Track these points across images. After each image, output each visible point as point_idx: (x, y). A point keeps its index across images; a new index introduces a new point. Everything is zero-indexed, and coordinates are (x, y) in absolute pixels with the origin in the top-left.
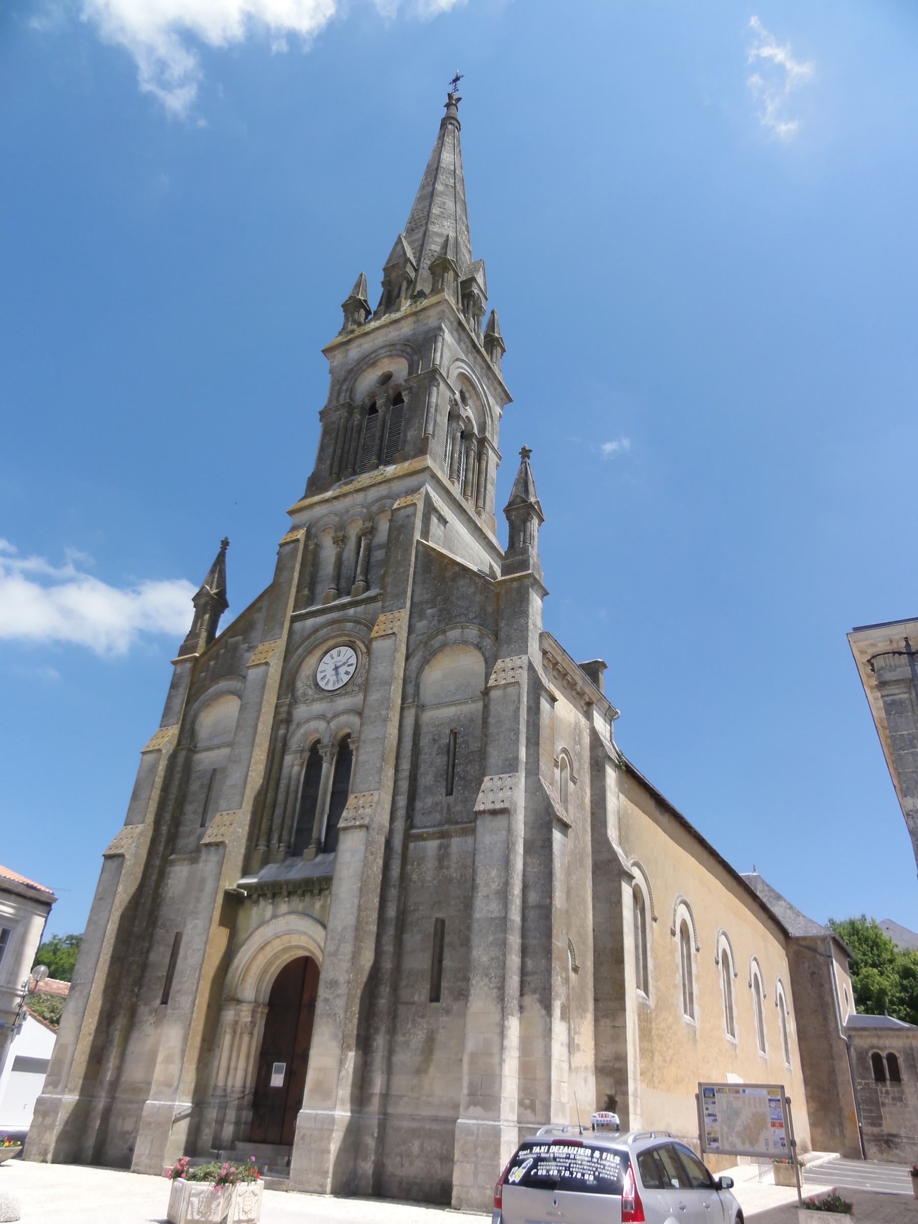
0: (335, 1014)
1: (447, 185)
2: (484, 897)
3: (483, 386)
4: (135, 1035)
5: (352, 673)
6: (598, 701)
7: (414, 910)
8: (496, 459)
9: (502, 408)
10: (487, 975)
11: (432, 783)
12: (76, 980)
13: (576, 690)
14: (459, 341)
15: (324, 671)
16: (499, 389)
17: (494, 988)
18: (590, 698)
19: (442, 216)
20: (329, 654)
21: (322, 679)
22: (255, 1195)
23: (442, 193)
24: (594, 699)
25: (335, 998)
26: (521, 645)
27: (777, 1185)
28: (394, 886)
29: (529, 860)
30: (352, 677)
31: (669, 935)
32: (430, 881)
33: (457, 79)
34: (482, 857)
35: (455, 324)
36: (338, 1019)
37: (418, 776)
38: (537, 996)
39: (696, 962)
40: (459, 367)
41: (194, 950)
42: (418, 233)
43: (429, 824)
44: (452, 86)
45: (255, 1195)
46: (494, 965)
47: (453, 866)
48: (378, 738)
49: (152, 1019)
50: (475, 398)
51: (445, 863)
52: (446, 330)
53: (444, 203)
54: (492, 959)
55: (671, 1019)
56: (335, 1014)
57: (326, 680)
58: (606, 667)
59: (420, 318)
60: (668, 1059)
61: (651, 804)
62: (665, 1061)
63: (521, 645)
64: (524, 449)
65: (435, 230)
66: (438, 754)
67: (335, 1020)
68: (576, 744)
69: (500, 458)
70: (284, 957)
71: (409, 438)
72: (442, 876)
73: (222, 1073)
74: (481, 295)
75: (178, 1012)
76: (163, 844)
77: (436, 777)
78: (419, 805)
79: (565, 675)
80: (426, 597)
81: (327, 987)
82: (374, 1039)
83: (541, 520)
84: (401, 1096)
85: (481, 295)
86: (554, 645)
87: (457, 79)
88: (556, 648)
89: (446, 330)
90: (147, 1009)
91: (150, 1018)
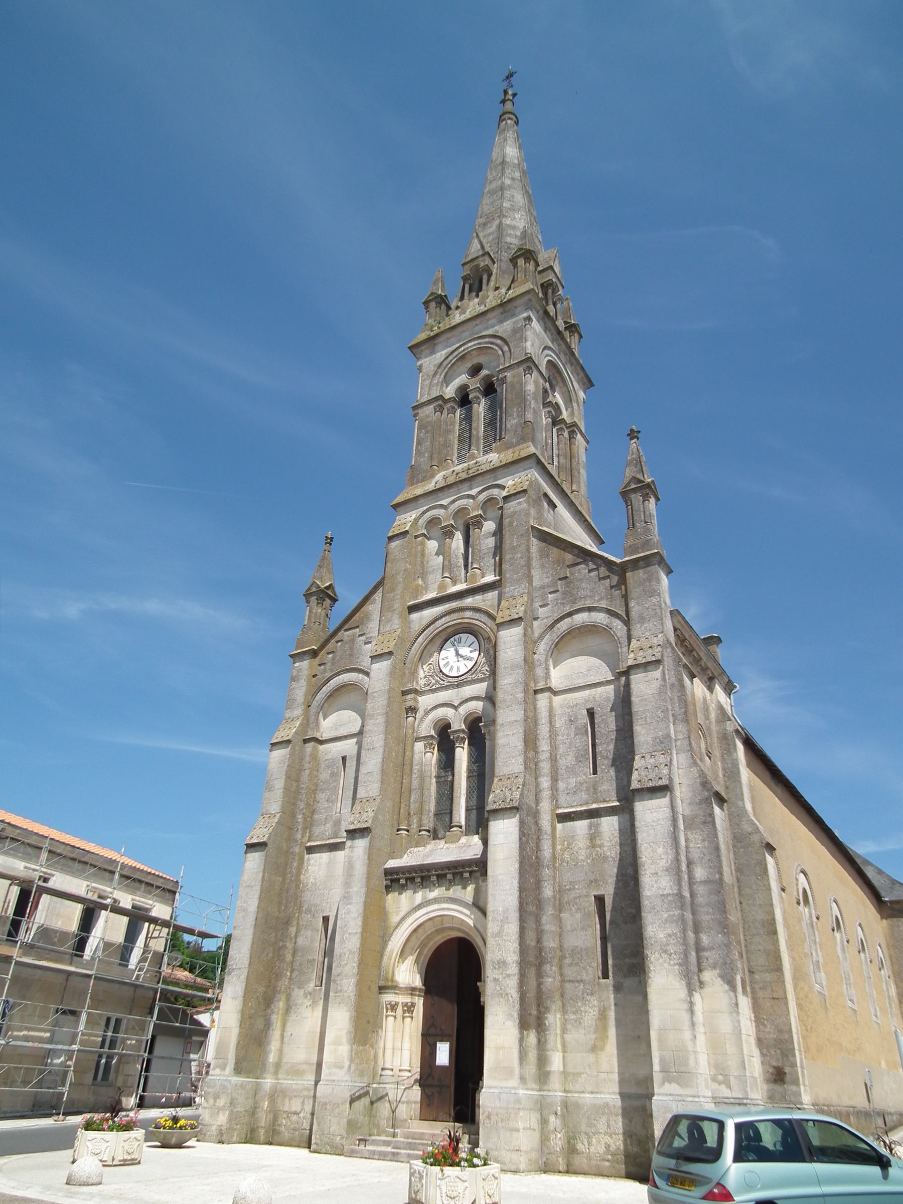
0: (507, 994)
1: (513, 179)
2: (653, 874)
3: (568, 372)
4: (293, 1017)
5: (476, 659)
6: (720, 675)
7: (570, 890)
8: (585, 443)
9: (585, 393)
10: (665, 952)
11: (573, 763)
12: (232, 965)
13: (701, 665)
14: (546, 329)
15: (446, 658)
16: (582, 375)
17: (675, 965)
18: (712, 673)
19: (512, 209)
20: (449, 641)
21: (444, 665)
22: (496, 1178)
23: (510, 187)
24: (716, 675)
25: (504, 978)
26: (655, 623)
27: (421, 1119)
28: (548, 866)
29: (690, 836)
30: (476, 663)
31: (796, 905)
32: (583, 861)
33: (511, 75)
34: (644, 835)
35: (541, 312)
36: (510, 998)
37: (558, 757)
38: (718, 971)
39: (818, 931)
40: (547, 356)
41: (350, 934)
42: (491, 227)
43: (575, 804)
44: (506, 83)
45: (496, 1178)
46: (672, 941)
47: (607, 844)
48: (516, 721)
49: (308, 1002)
50: (561, 384)
51: (598, 842)
52: (534, 319)
53: (513, 196)
54: (670, 936)
55: (806, 988)
56: (507, 994)
57: (450, 667)
58: (721, 641)
59: (506, 309)
60: (809, 1028)
61: (767, 775)
62: (807, 1030)
63: (655, 623)
64: (632, 430)
65: (508, 223)
66: (576, 735)
67: (508, 1000)
68: (706, 720)
69: (588, 442)
70: (436, 939)
71: (508, 426)
72: (596, 855)
73: (389, 1053)
74: (558, 283)
75: (341, 994)
76: (300, 831)
77: (577, 758)
78: (561, 785)
79: (692, 651)
80: (546, 580)
81: (495, 968)
82: (546, 1018)
83: (657, 499)
84: (579, 1074)
85: (558, 283)
86: (682, 622)
87: (511, 75)
88: (684, 624)
89: (534, 319)
90: (302, 992)
91: (305, 1001)
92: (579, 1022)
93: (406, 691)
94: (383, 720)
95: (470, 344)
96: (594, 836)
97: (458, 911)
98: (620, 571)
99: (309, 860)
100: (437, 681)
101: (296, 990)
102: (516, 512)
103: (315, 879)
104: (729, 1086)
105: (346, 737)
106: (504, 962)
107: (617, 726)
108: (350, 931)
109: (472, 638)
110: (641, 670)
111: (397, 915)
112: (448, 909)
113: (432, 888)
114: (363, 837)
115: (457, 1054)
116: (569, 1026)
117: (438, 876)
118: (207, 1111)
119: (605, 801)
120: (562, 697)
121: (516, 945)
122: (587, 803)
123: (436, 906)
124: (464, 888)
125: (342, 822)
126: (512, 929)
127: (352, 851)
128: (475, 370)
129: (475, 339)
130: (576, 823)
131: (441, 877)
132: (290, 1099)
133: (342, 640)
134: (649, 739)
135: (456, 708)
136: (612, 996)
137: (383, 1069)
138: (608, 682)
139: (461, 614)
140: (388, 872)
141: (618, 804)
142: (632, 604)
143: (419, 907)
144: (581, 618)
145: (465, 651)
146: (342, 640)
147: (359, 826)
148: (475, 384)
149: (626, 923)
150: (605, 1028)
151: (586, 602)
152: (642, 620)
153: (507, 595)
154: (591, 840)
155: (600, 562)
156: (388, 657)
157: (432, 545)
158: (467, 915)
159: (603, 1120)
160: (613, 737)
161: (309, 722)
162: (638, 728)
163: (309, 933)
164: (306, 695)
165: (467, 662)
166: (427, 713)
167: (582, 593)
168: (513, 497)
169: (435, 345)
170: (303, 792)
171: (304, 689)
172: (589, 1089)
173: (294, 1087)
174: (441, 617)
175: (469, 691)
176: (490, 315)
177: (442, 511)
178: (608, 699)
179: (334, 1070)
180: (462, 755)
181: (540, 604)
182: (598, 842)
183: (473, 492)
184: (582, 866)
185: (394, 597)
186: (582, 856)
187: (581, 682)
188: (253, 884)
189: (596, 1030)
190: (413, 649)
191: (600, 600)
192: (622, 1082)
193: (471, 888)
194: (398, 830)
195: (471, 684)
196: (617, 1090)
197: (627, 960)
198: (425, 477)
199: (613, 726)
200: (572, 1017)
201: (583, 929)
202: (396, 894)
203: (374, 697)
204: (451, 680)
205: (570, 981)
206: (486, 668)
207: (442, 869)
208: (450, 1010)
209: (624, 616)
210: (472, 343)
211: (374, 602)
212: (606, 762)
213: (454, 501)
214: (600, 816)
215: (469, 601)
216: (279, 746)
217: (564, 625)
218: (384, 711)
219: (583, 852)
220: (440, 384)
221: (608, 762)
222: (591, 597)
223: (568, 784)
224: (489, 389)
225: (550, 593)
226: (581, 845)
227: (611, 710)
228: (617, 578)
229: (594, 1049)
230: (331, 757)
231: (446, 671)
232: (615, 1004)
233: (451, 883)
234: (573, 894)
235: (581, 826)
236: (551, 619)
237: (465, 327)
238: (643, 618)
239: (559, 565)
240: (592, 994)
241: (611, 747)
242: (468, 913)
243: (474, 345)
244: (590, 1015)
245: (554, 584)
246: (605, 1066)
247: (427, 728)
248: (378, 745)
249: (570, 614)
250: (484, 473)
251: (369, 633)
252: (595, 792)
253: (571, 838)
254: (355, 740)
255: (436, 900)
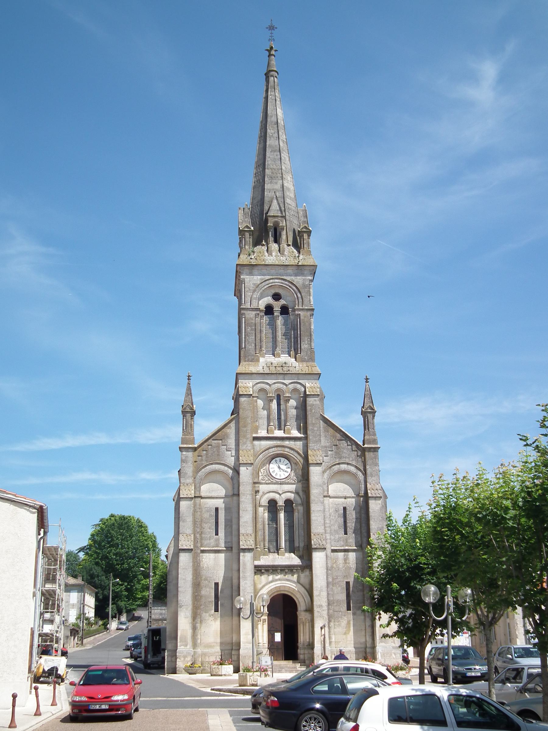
49: (212, 618)
77: (339, 527)
84: (340, 642)
92: (340, 625)
93: (255, 482)
94: (251, 497)
95: (276, 281)
96: (346, 559)
97: (290, 584)
99: (202, 556)
100: (269, 479)
101: (204, 614)
105: (217, 498)
106: (321, 605)
107: (356, 516)
108: (248, 591)
109: (286, 461)
112: (285, 583)
113: (277, 575)
114: (249, 552)
115: (285, 637)
117: (281, 570)
119: (350, 546)
120: (332, 499)
123: (279, 582)
125: (220, 540)
127: (244, 558)
128: (277, 297)
129: (279, 279)
132: (209, 657)
133: (211, 445)
134: (376, 527)
135: (280, 495)
137: (258, 643)
138: (353, 497)
139: (283, 449)
141: (356, 548)
142: (368, 467)
143: (272, 582)
144: (344, 467)
145: (283, 467)
146: (211, 445)
148: (277, 306)
149: (358, 592)
150: (350, 627)
151: (346, 460)
152: (372, 476)
153: (311, 448)
155: (353, 442)
157: (260, 403)
160: (354, 521)
162: (372, 522)
163: (208, 589)
164: (193, 472)
165: (285, 473)
166: (264, 494)
167: (344, 455)
174: (272, 448)
176: (289, 268)
177: (268, 387)
178: (352, 504)
180: (282, 516)
184: (341, 570)
185: (246, 430)
186: (341, 566)
188: (187, 567)
191: (352, 460)
192: (354, 644)
195: (287, 484)
196: (353, 646)
197: (358, 605)
198: (253, 359)
199: (354, 516)
200: (337, 623)
201: (341, 593)
202: (259, 576)
203: (244, 485)
204: (277, 480)
205: (336, 611)
207: (282, 567)
209: (362, 470)
210: (278, 281)
211: (230, 428)
213: (275, 383)
215: (287, 443)
217: (336, 468)
219: (341, 565)
220: (257, 299)
221: (352, 531)
222: (348, 458)
223: (335, 537)
225: (329, 451)
226: (341, 562)
227: (354, 510)
228: (360, 452)
229: (345, 634)
231: (274, 475)
232: (353, 619)
234: (337, 580)
235: (341, 555)
237: (270, 266)
238: (372, 475)
239: (333, 438)
240: (345, 616)
241: (354, 525)
242: (295, 585)
243: (279, 282)
244: (344, 622)
245: (331, 447)
246: (349, 639)
247: (264, 501)
249: (339, 464)
253: (337, 559)
255: (279, 580)
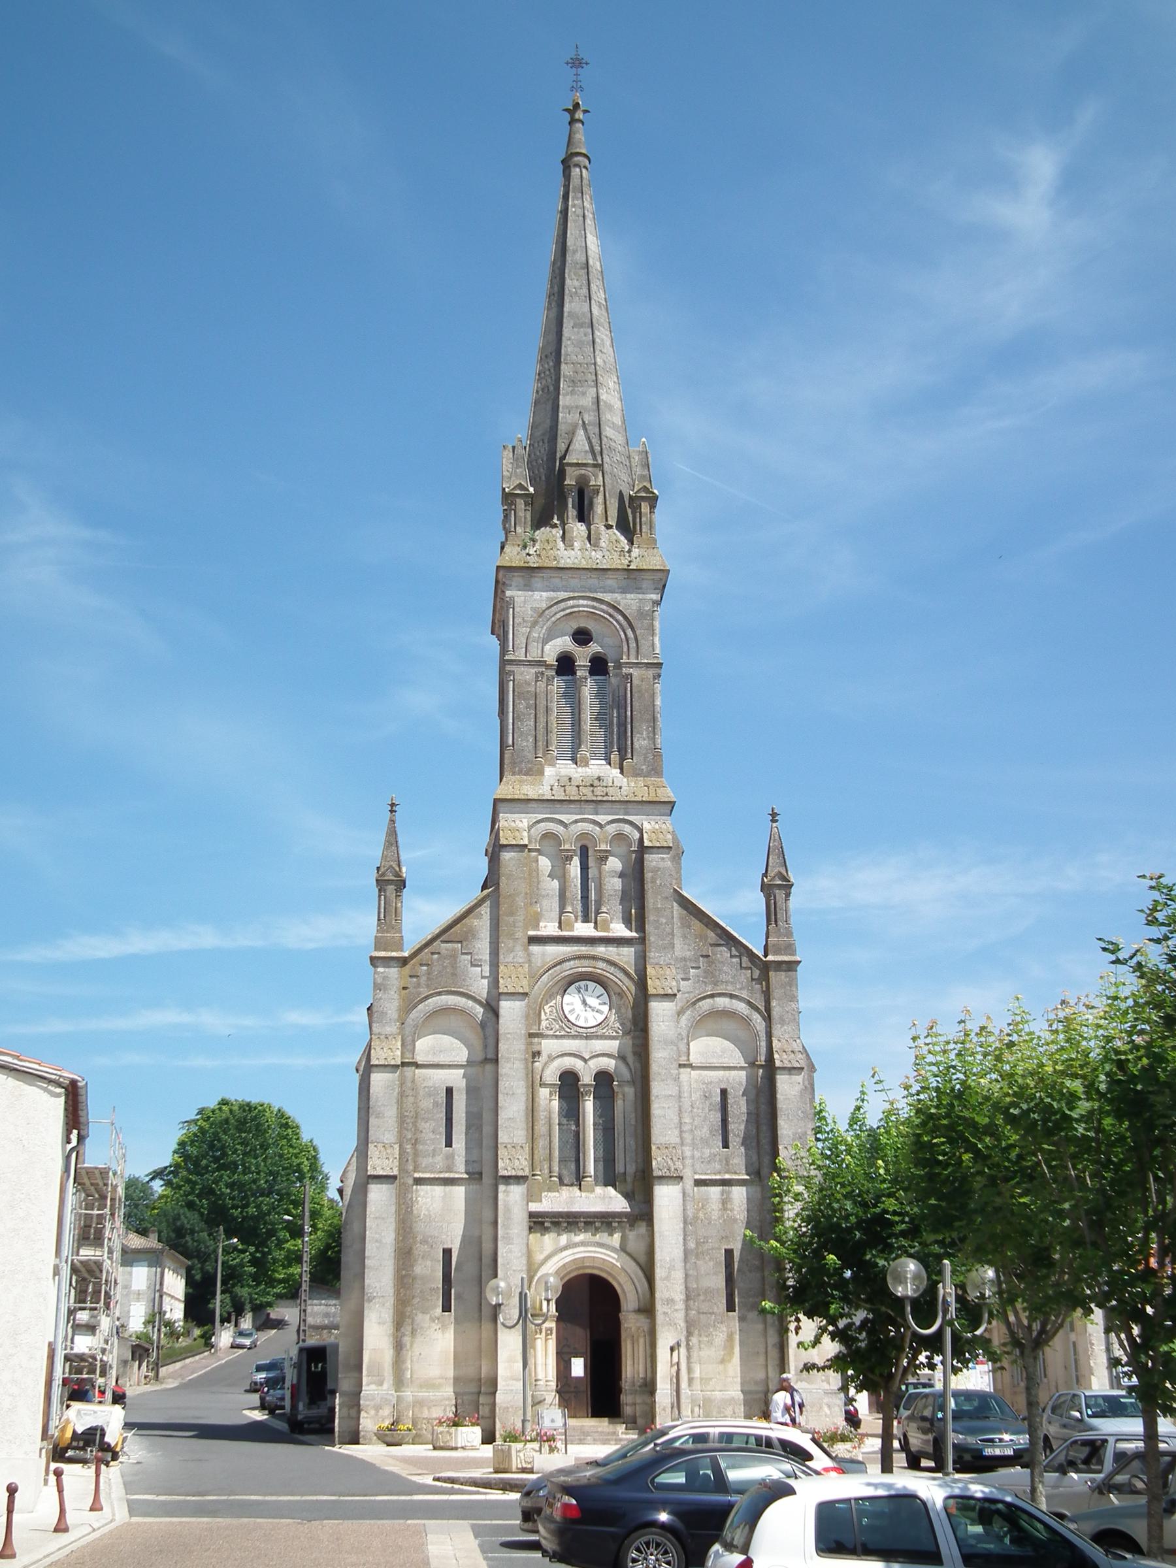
48: (671, 1096)
51: (729, 1206)
77: (711, 1131)
84: (711, 1379)
92: (710, 1343)
95: (581, 602)
96: (725, 1202)
97: (605, 1254)
98: (766, 968)
100: (562, 1027)
102: (659, 868)
103: (428, 1210)
104: (829, 1383)
105: (450, 1066)
106: (672, 1301)
109: (600, 990)
110: (786, 1072)
111: (541, 1253)
112: (595, 1252)
114: (518, 1184)
115: (593, 1368)
116: (702, 1346)
118: (369, 1420)
119: (736, 1173)
120: (698, 1072)
121: (683, 1287)
122: (720, 1173)
123: (582, 1249)
124: (611, 1235)
126: (679, 1275)
127: (507, 1196)
128: (582, 637)
130: (709, 1188)
131: (556, 1224)
132: (429, 1408)
133: (439, 953)
135: (585, 1061)
136: (737, 1324)
138: (742, 1068)
139: (593, 963)
140: (532, 1215)
141: (748, 1177)
142: (774, 1003)
143: (565, 1248)
144: (722, 1002)
145: (592, 1001)
146: (439, 953)
147: (514, 1173)
148: (582, 657)
149: (750, 1271)
150: (732, 1348)
151: (728, 988)
152: (782, 1022)
153: (652, 960)
154: (723, 1204)
155: (742, 950)
156: (521, 997)
157: (545, 863)
158: (614, 1258)
159: (730, 1408)
160: (745, 1119)
161: (1091, 1298)
162: (782, 1123)
163: (429, 1263)
164: (400, 1010)
166: (551, 1059)
168: (655, 850)
169: (531, 577)
170: (408, 1121)
171: (396, 1003)
172: (718, 1388)
173: (432, 1398)
174: (569, 960)
175: (599, 1045)
177: (561, 829)
178: (740, 1083)
179: (511, 1382)
180: (589, 1106)
181: (682, 976)
182: (729, 1206)
183: (600, 818)
186: (715, 1215)
187: (715, 1062)
189: (725, 1348)
190: (536, 987)
191: (741, 989)
192: (742, 1384)
193: (617, 1236)
194: (551, 1177)
198: (530, 769)
199: (744, 1109)
200: (705, 1339)
201: (715, 1274)
202: (539, 1235)
203: (508, 1039)
204: (579, 1029)
206: (618, 1025)
208: (581, 1336)
209: (763, 1009)
210: (585, 602)
211: (480, 916)
212: (738, 1140)
213: (576, 821)
214: (732, 1185)
215: (601, 950)
216: (382, 1069)
217: (706, 1005)
218: (523, 1057)
221: (739, 1140)
222: (732, 983)
223: (703, 1153)
224: (599, 666)
225: (692, 968)
226: (714, 1207)
227: (743, 1095)
229: (722, 1361)
230: (431, 1085)
231: (572, 1018)
233: (597, 1230)
234: (706, 1247)
235: (715, 1191)
236: (692, 995)
238: (783, 1020)
241: (743, 1127)
242: (616, 1256)
243: (587, 606)
244: (720, 1337)
246: (731, 1372)
247: (551, 1075)
248: (519, 1091)
249: (712, 996)
250: (615, 801)
251: (477, 954)
252: (727, 1163)
253: (706, 1200)
254: (462, 1071)
255: (582, 1244)
